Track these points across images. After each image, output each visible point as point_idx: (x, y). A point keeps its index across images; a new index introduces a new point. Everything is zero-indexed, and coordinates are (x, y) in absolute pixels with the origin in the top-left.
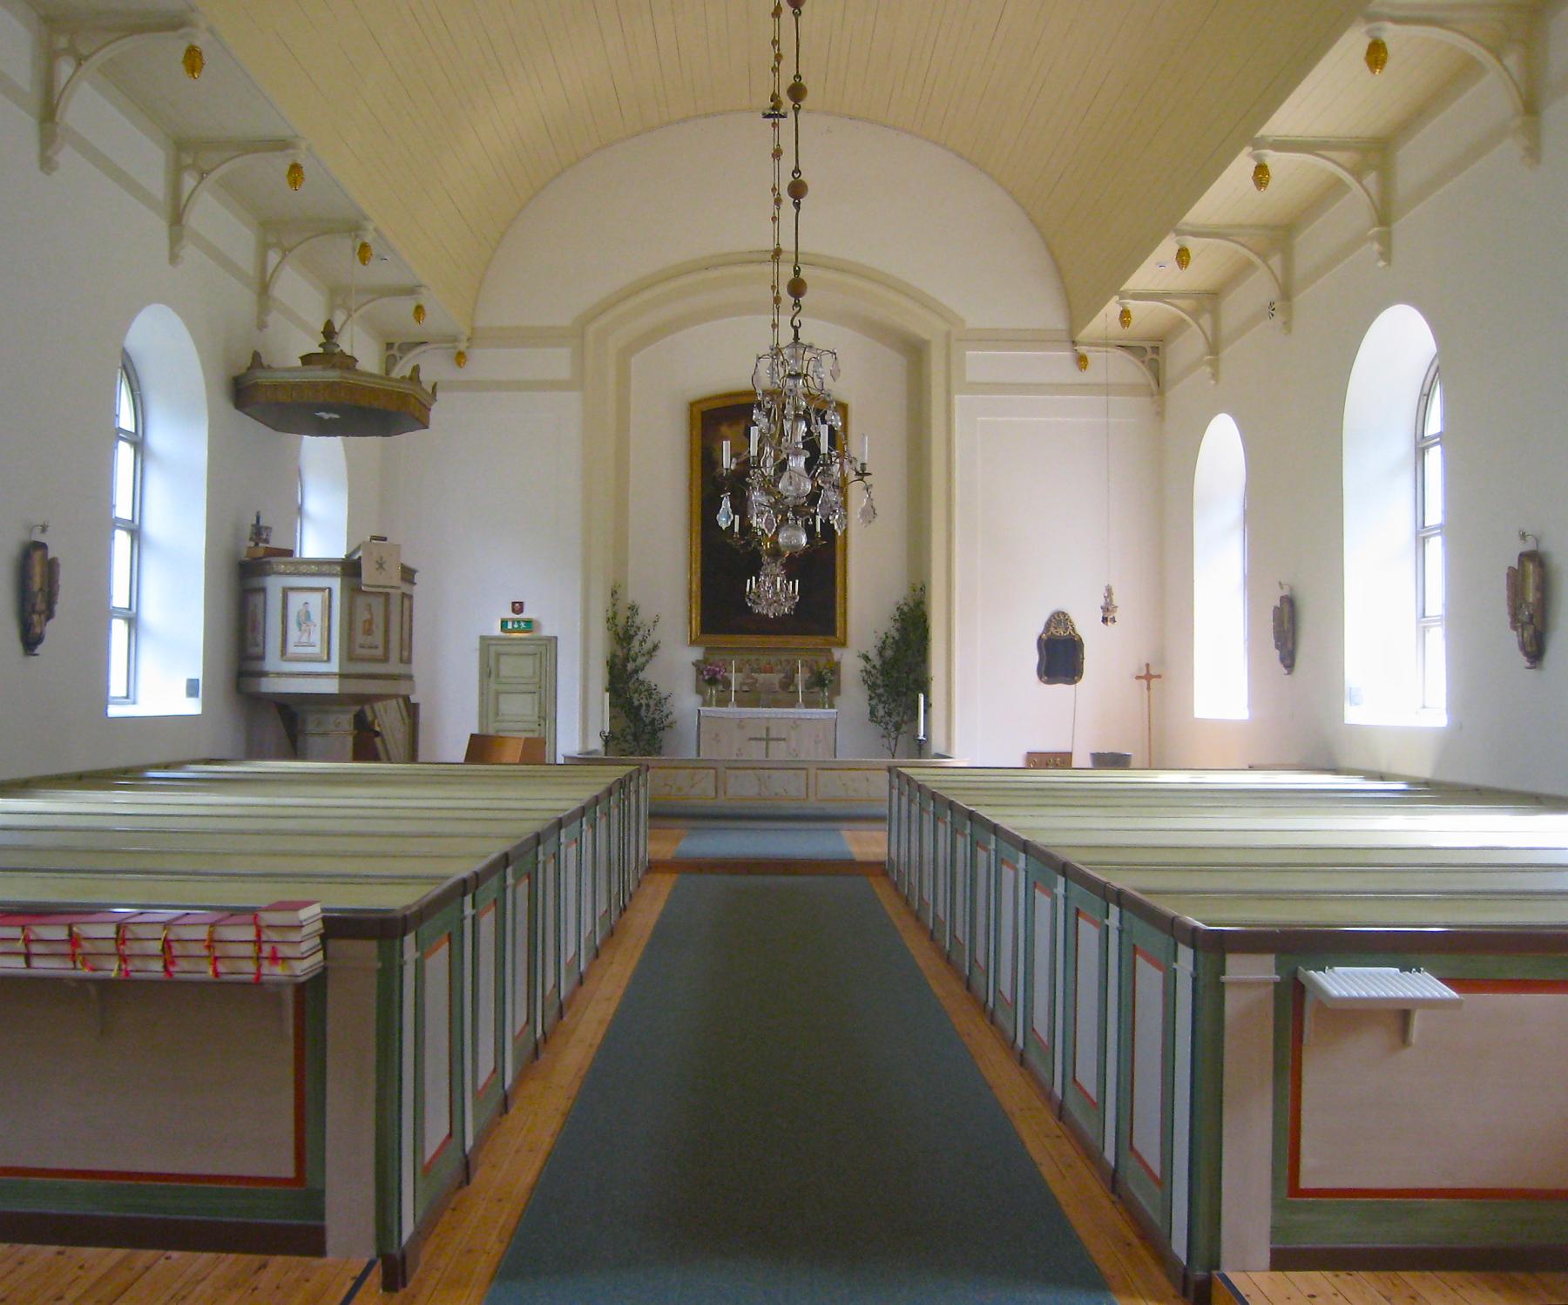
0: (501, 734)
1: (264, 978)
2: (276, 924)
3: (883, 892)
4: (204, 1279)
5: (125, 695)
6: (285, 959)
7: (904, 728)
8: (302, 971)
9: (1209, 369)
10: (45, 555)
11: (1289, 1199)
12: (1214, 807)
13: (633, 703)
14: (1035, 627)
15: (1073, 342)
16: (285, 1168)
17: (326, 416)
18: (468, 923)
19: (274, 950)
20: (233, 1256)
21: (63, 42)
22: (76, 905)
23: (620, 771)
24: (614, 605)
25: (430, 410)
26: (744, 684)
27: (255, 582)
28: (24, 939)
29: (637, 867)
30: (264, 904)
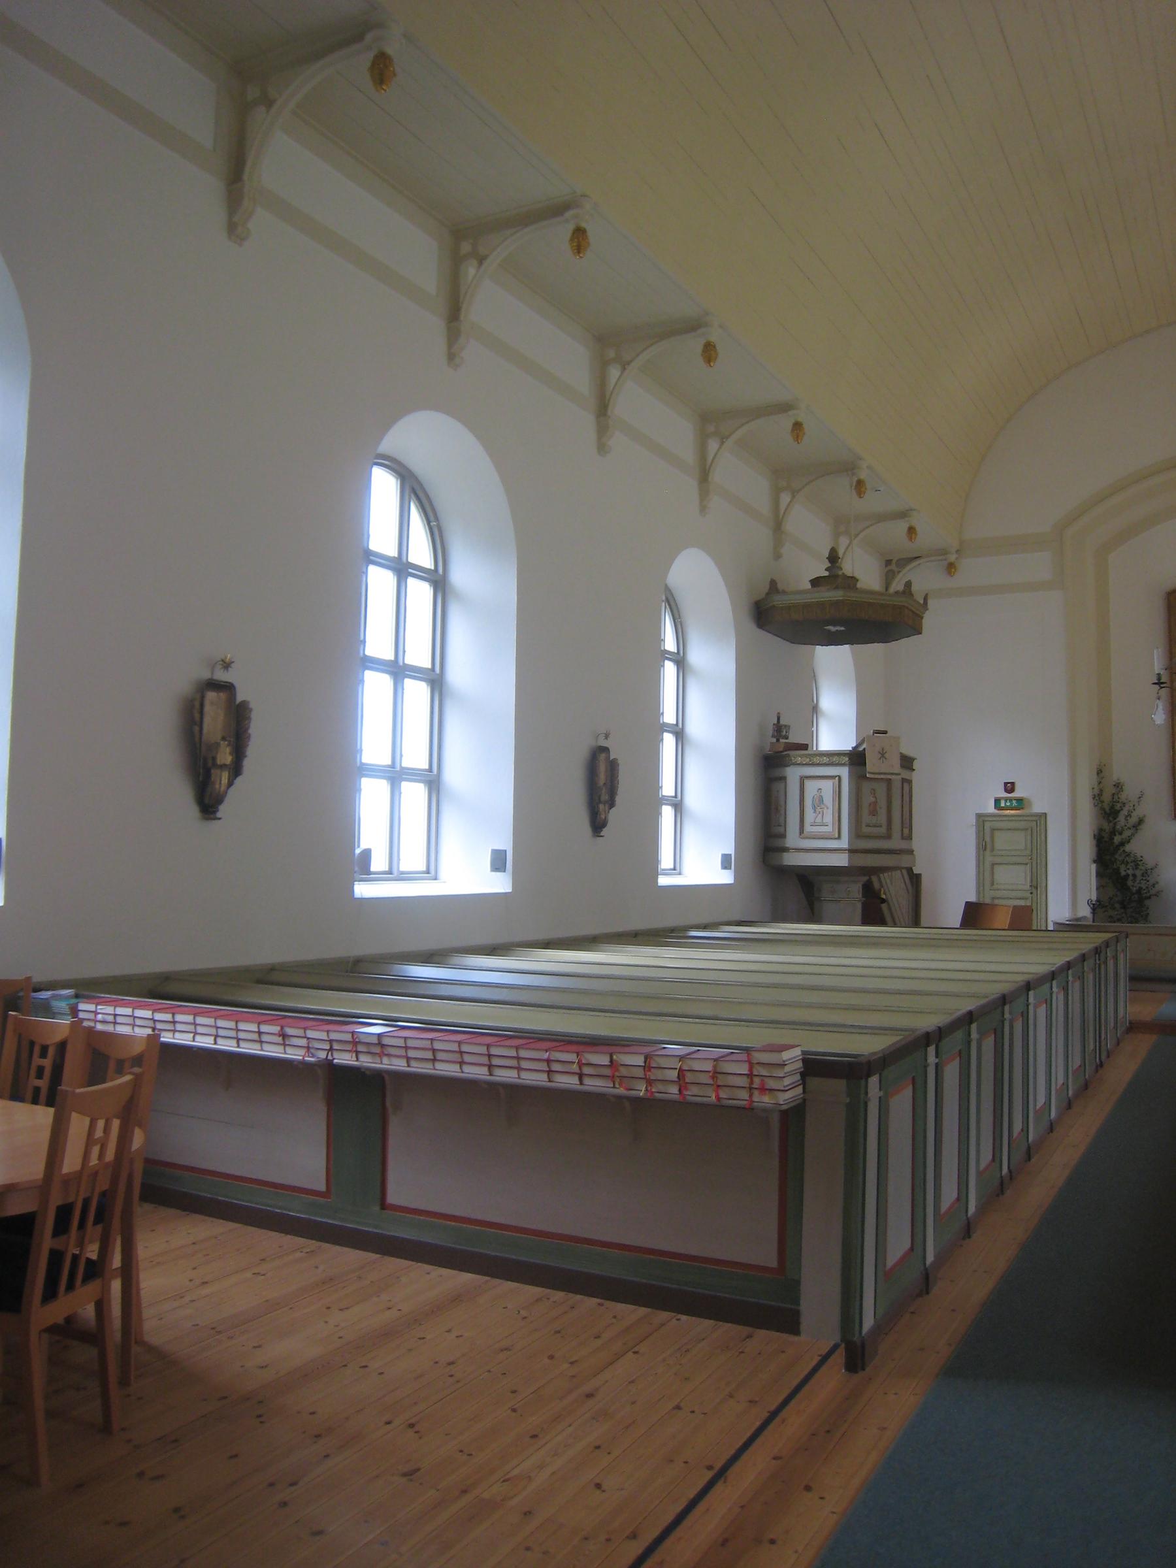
0: (996, 902)
5: (672, 867)
6: (771, 1090)
13: (1120, 873)
17: (832, 628)
21: (611, 354)
23: (1099, 938)
25: (922, 618)
27: (777, 772)
28: (578, 1062)
29: (1116, 1027)
30: (758, 1045)
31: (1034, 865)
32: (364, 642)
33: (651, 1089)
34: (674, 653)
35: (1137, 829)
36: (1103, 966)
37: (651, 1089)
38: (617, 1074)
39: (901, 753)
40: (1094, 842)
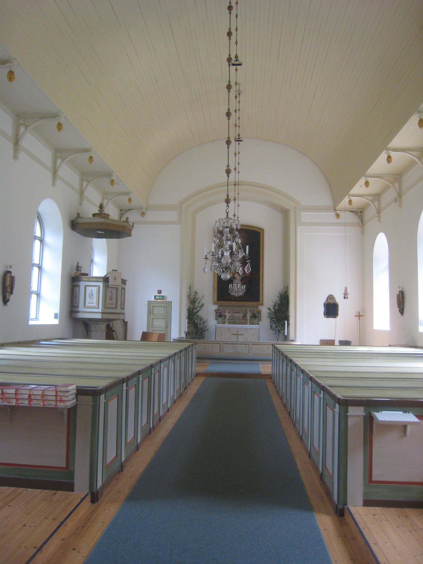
0: (154, 332)
1: (58, 406)
2: (61, 391)
3: (269, 384)
4: (36, 497)
6: (64, 401)
7: (281, 331)
8: (69, 405)
9: (377, 218)
10: (11, 275)
11: (369, 484)
12: (376, 359)
14: (323, 300)
15: (335, 210)
16: (63, 464)
17: (99, 232)
18: (124, 392)
19: (61, 398)
20: (46, 491)
21: (22, 121)
22: (32, 384)
23: (186, 345)
24: (190, 291)
25: (132, 231)
26: (231, 317)
27: (77, 283)
29: (192, 375)
31: (167, 319)
32: (35, 232)
33: (18, 402)
34: (39, 237)
35: (202, 308)
36: (187, 354)
37: (18, 402)
38: (4, 397)
39: (122, 278)
40: (187, 312)
